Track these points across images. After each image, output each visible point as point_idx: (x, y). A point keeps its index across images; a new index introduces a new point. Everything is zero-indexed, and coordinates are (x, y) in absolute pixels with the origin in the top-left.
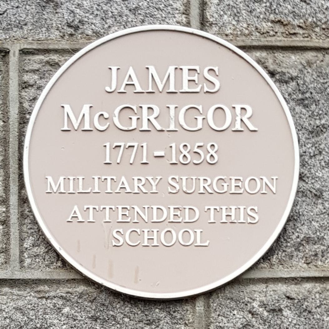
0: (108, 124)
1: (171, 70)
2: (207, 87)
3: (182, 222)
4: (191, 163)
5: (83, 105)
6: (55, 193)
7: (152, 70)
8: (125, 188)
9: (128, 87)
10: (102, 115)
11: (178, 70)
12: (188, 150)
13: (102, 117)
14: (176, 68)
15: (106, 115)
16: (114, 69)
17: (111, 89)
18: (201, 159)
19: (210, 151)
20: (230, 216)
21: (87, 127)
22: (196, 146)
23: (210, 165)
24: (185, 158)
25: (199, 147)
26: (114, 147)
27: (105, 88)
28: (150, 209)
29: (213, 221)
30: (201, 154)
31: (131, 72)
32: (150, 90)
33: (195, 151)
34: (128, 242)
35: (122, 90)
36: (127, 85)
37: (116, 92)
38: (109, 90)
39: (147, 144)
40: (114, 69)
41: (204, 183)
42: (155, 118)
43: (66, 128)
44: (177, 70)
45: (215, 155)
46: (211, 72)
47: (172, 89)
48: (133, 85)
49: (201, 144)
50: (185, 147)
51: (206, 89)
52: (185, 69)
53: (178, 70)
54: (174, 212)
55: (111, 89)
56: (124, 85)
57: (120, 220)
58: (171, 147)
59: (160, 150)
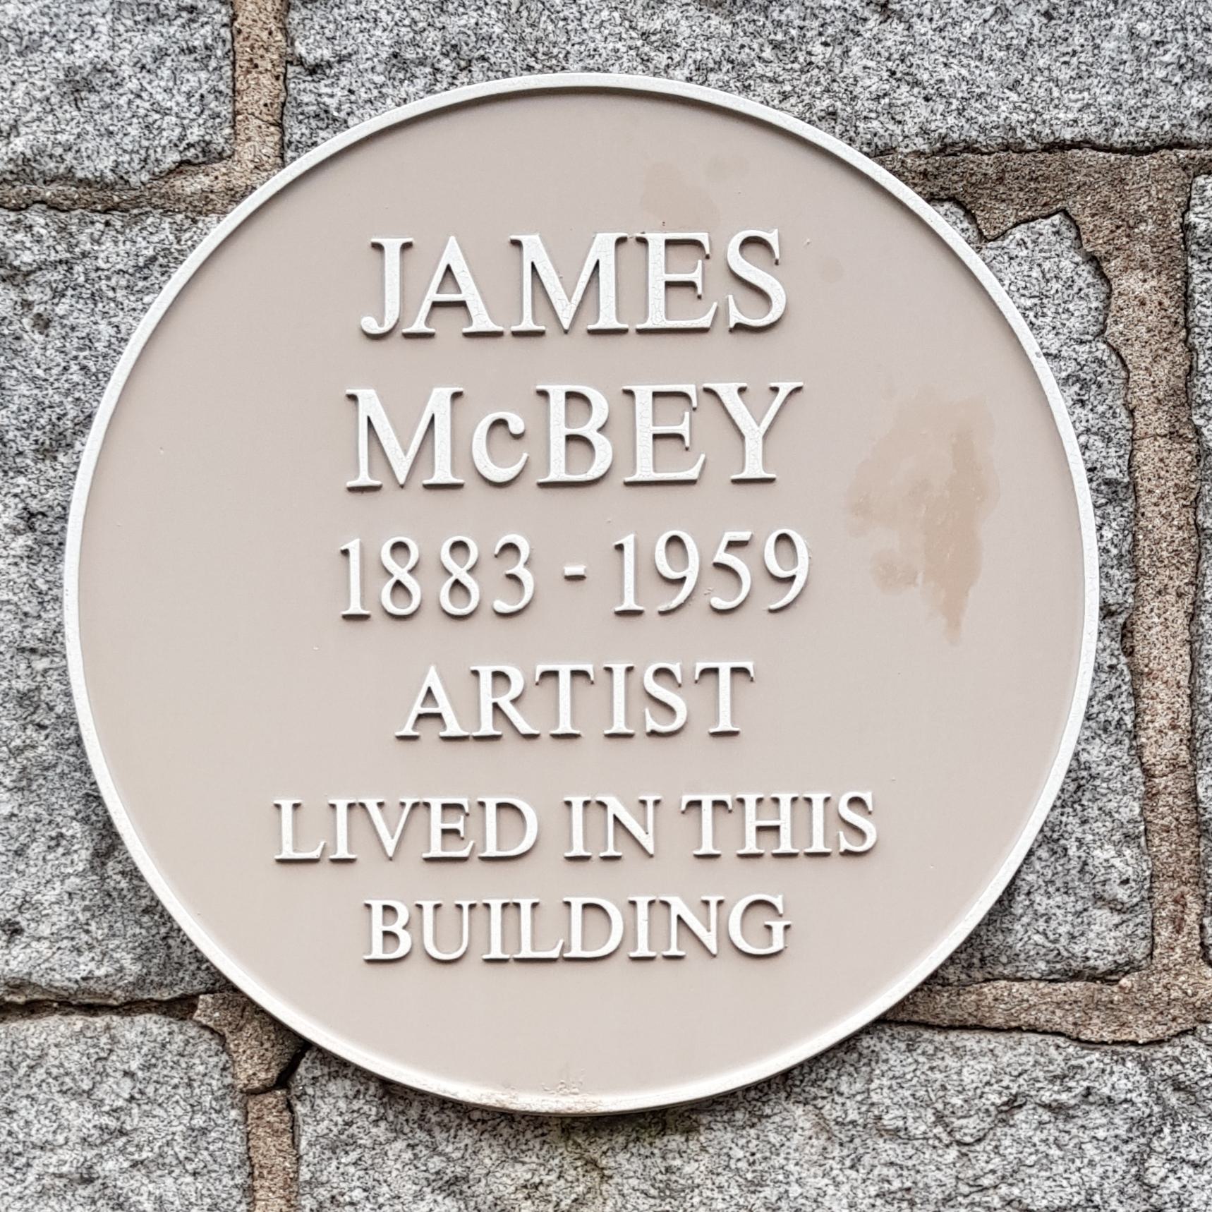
0: (525, 456)
1: (603, 248)
2: (738, 308)
3: (475, 859)
4: (485, 613)
5: (431, 388)
6: (391, 859)
7: (534, 249)
8: (439, 716)
9: (440, 312)
10: (501, 423)
11: (631, 247)
12: (411, 563)
13: (499, 430)
14: (621, 241)
15: (516, 425)
16: (392, 246)
17: (381, 324)
18: (520, 599)
19: (391, 570)
20: (776, 829)
21: (443, 474)
22: (724, 544)
23: (399, 624)
24: (400, 593)
25: (732, 545)
26: (497, 551)
27: (360, 321)
28: (801, 803)
29: (822, 849)
30: (522, 579)
31: (453, 255)
32: (527, 324)
33: (716, 560)
34: (740, 946)
35: (419, 326)
36: (435, 305)
37: (398, 334)
38: (375, 329)
39: (361, 544)
40: (392, 246)
41: (495, 692)
42: (600, 430)
43: (364, 479)
44: (624, 248)
45: (408, 581)
46: (754, 250)
47: (607, 320)
48: (462, 304)
49: (743, 536)
50: (460, 551)
51: (736, 317)
52: (644, 394)
53: (631, 247)
54: (443, 821)
55: (381, 324)
56: (426, 306)
57: (436, 852)
58: (620, 548)
59: (574, 562)
